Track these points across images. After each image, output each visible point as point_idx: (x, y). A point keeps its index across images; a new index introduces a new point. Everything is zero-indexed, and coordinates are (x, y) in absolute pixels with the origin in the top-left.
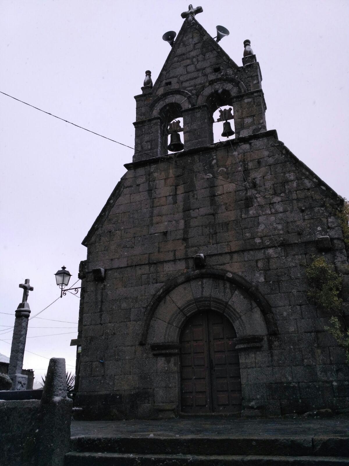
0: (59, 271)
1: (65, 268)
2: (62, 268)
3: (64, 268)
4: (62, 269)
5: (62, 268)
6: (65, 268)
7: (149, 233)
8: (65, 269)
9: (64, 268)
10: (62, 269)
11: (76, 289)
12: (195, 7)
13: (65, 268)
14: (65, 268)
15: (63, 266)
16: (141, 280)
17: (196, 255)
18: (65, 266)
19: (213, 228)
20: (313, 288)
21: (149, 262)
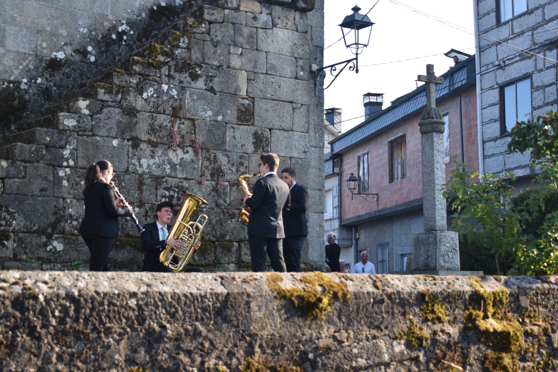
0: (347, 18)
1: (359, 9)
2: (353, 9)
3: (356, 9)
4: (352, 12)
5: (353, 9)
6: (359, 9)
7: (546, 66)
8: (360, 12)
9: (356, 9)
10: (352, 12)
11: (332, 66)
12: (424, 73)
13: (359, 9)
14: (359, 9)
15: (353, 6)
16: (70, 237)
17: (213, 310)
18: (359, 6)
19: (28, 124)
20: (293, 347)
21: (513, 33)
